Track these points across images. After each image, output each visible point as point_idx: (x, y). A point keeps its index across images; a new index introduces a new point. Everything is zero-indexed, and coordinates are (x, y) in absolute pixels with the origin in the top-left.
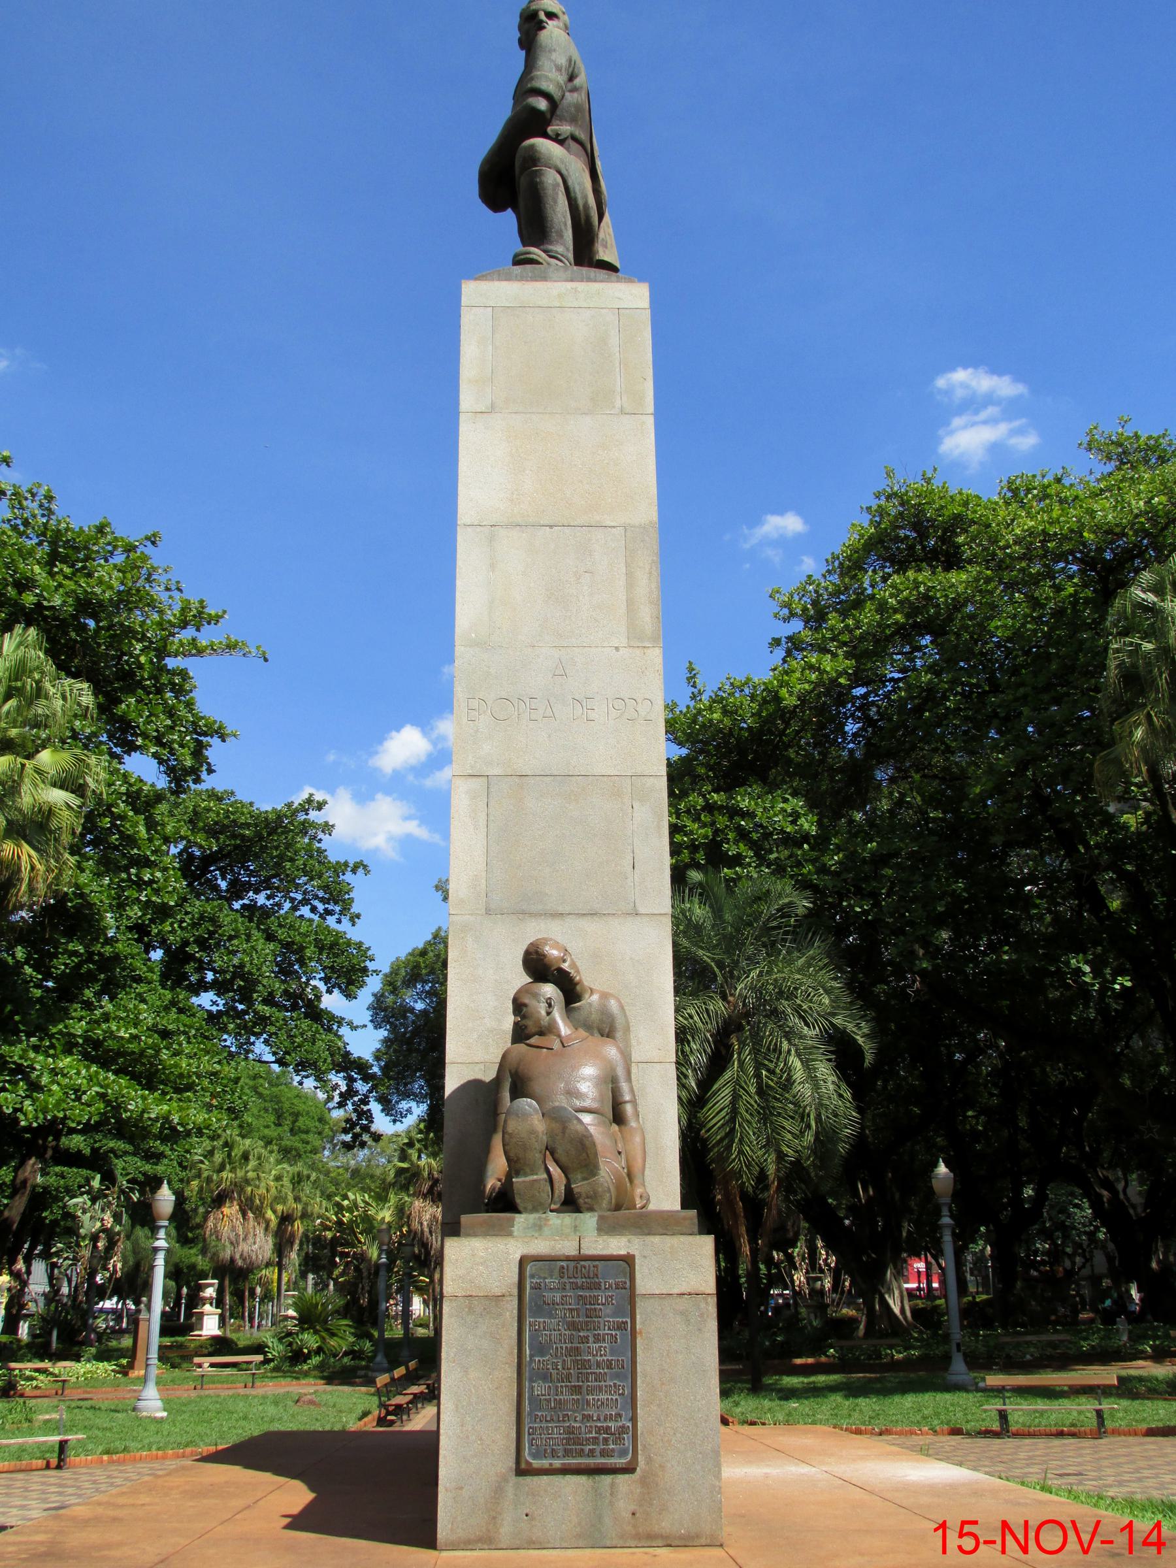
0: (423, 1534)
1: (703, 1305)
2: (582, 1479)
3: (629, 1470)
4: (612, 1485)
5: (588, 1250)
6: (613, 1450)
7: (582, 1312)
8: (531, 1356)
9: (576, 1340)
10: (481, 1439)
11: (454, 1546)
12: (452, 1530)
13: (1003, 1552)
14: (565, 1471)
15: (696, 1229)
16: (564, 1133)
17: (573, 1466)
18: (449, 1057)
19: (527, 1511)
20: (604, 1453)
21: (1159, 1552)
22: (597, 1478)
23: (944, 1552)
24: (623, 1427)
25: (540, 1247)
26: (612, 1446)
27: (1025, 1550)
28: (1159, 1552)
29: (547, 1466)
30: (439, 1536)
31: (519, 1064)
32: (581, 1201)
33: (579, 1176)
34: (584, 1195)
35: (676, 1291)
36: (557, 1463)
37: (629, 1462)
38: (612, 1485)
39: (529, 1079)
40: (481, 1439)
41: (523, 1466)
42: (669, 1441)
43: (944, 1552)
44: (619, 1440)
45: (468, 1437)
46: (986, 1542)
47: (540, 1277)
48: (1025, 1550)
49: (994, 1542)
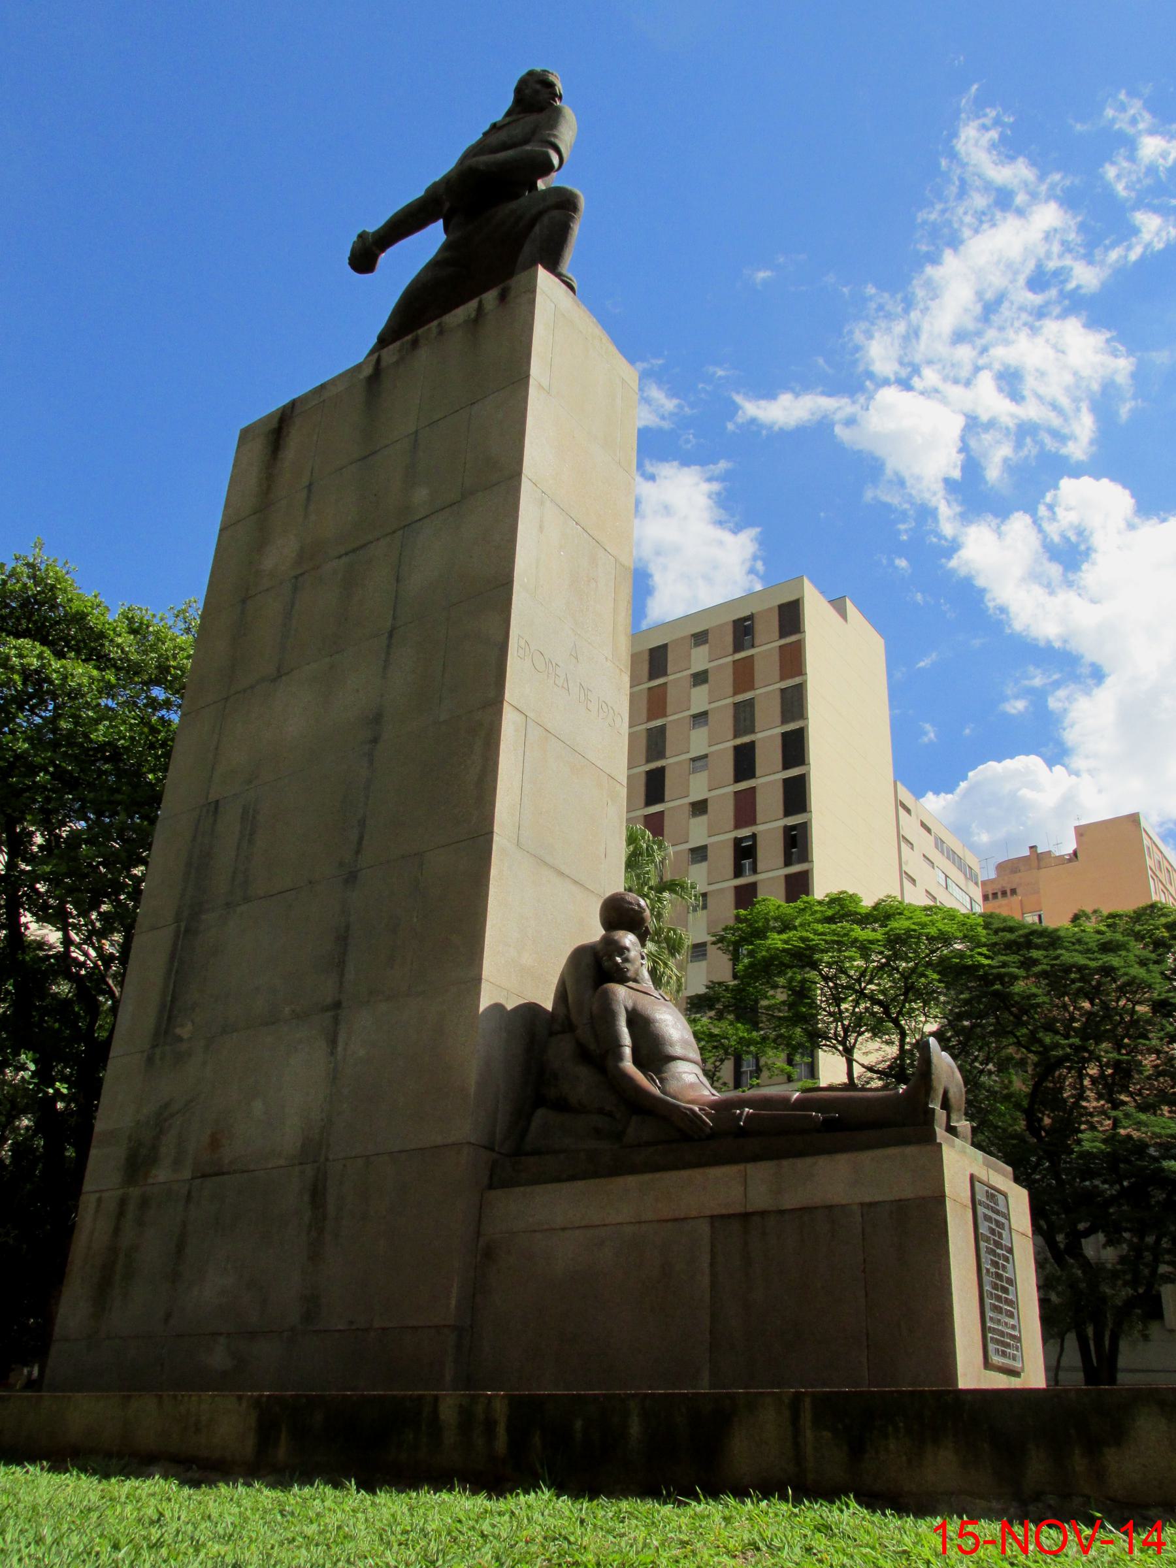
18: (485, 973)
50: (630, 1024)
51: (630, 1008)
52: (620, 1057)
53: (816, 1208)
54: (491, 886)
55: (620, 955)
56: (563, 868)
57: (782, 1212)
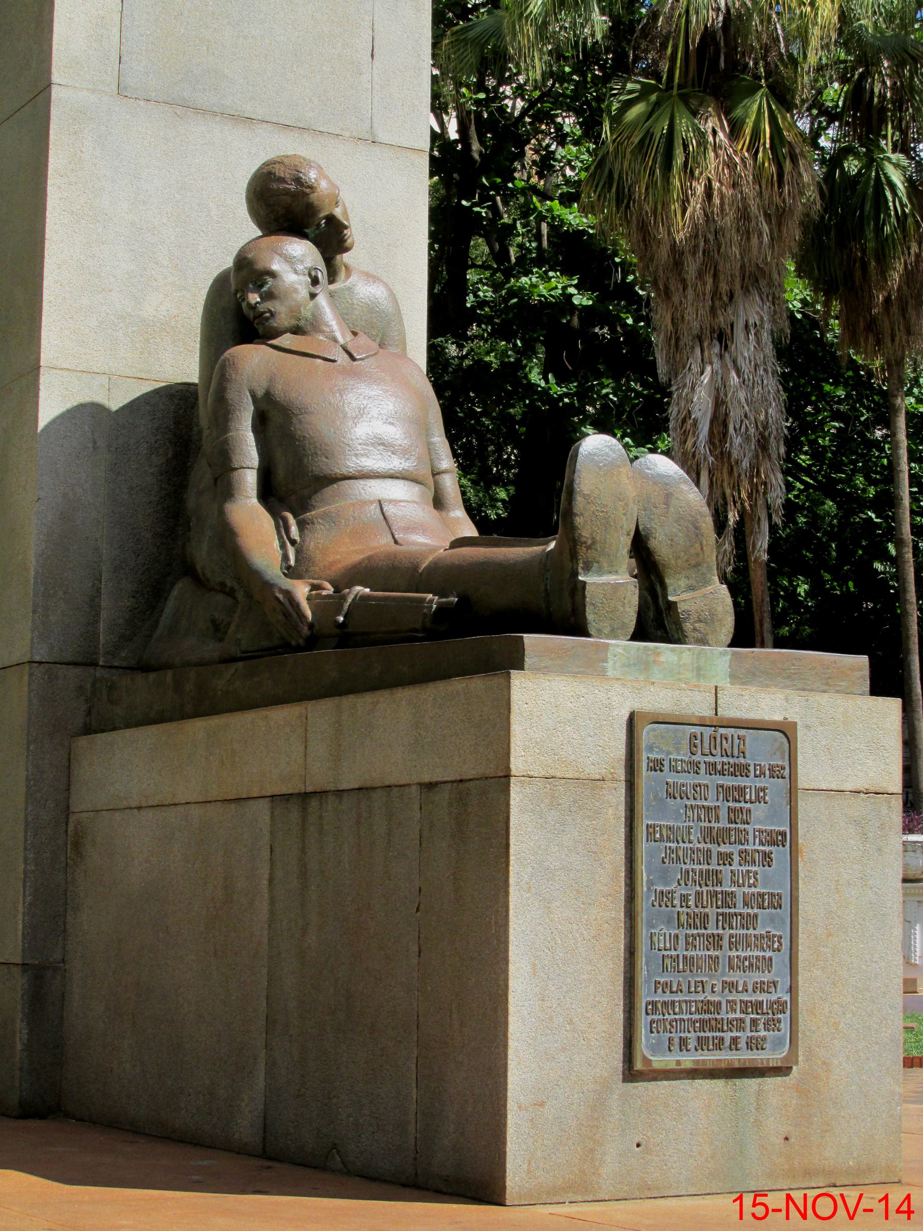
0: (477, 1182)
1: (884, 811)
2: (718, 1085)
3: (781, 1071)
4: (759, 1093)
5: (728, 712)
6: (764, 1039)
7: (723, 813)
8: (650, 883)
9: (714, 859)
10: (571, 1022)
11: (551, 1196)
12: (529, 1172)
13: (788, 1218)
14: (694, 1073)
15: (867, 688)
16: (667, 504)
17: (709, 1066)
18: (46, 357)
19: (636, 1141)
20: (755, 1044)
21: (909, 1218)
22: (738, 1082)
23: (741, 1218)
24: (777, 1002)
25: (658, 698)
26: (763, 1033)
27: (804, 1216)
28: (909, 1218)
29: (673, 1066)
30: (509, 1183)
31: (272, 380)
32: (688, 626)
33: (683, 583)
34: (694, 616)
35: (849, 786)
36: (688, 1060)
37: (785, 1059)
38: (759, 1093)
39: (304, 410)
40: (571, 1022)
41: (639, 1066)
42: (836, 1024)
43: (741, 1218)
44: (772, 1024)
45: (551, 1018)
46: (774, 1210)
47: (661, 751)
48: (804, 1216)
49: (780, 1210)
50: (261, 422)
51: (260, 393)
52: (224, 487)
53: (373, 789)
54: (50, 189)
55: (259, 287)
56: (248, 109)
57: (339, 793)
